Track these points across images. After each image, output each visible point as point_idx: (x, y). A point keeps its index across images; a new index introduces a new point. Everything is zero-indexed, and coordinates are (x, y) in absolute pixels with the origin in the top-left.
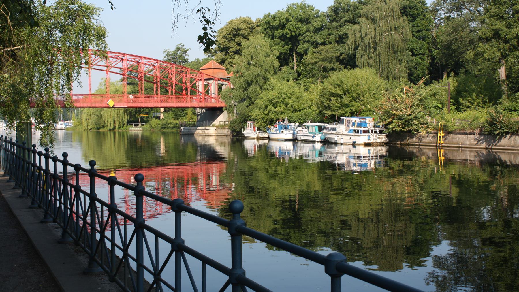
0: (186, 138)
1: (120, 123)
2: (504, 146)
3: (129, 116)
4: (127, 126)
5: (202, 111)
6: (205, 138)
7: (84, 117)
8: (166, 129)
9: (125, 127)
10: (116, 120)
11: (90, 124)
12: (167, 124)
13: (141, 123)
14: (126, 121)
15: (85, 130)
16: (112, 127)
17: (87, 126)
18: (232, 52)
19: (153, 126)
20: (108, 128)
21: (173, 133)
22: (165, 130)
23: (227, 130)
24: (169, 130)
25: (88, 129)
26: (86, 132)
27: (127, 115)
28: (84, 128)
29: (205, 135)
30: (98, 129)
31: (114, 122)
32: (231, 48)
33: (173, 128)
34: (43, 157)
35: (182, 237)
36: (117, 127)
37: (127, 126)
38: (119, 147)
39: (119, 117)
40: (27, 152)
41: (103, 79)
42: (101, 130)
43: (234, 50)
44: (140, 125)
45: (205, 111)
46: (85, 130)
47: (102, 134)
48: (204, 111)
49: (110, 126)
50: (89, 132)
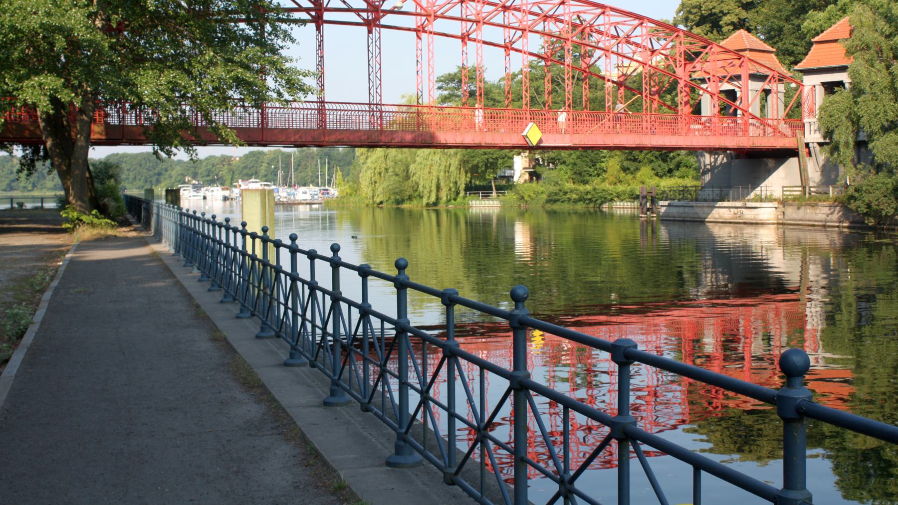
0: (676, 229)
1: (450, 189)
2: (793, 229)
3: (469, 175)
4: (464, 197)
5: (716, 160)
6: (741, 230)
7: (365, 179)
8: (559, 203)
9: (459, 200)
10: (442, 184)
11: (377, 193)
12: (561, 194)
13: (497, 190)
14: (463, 186)
15: (367, 205)
16: (433, 199)
17: (373, 197)
18: (728, 25)
19: (526, 198)
20: (425, 201)
21: (576, 213)
22: (556, 207)
23: (826, 210)
24: (566, 207)
25: (374, 202)
26: (371, 209)
27: (466, 173)
28: (367, 202)
29: (745, 223)
30: (398, 202)
31: (438, 188)
32: (725, 15)
33: (576, 201)
34: (239, 235)
35: (281, 264)
36: (444, 199)
37: (464, 197)
38: (449, 246)
39: (449, 177)
40: (217, 229)
41: (403, 97)
42: (406, 206)
43: (735, 20)
44: (494, 194)
45: (725, 160)
46: (367, 205)
47: (407, 214)
48: (721, 159)
49: (429, 197)
50: (378, 211)
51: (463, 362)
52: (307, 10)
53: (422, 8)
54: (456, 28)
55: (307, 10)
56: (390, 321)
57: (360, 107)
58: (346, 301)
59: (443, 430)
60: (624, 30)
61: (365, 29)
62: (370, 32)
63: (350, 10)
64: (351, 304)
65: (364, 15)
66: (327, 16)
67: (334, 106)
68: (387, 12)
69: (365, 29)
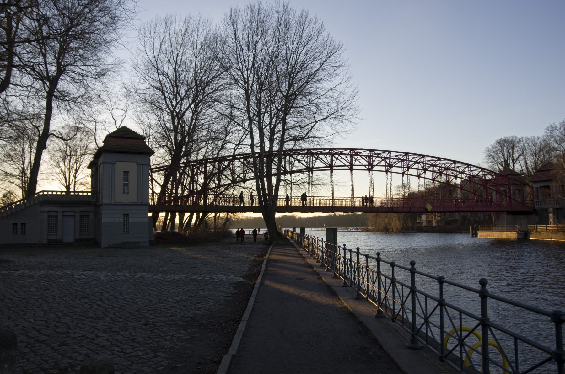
51: (397, 284)
52: (348, 166)
53: (388, 164)
54: (400, 170)
55: (348, 166)
56: (389, 278)
57: (348, 198)
58: (383, 275)
59: (410, 319)
60: (461, 169)
61: (368, 171)
62: (369, 172)
63: (362, 165)
64: (386, 277)
65: (367, 167)
66: (354, 167)
67: (357, 199)
68: (375, 166)
69: (368, 171)
